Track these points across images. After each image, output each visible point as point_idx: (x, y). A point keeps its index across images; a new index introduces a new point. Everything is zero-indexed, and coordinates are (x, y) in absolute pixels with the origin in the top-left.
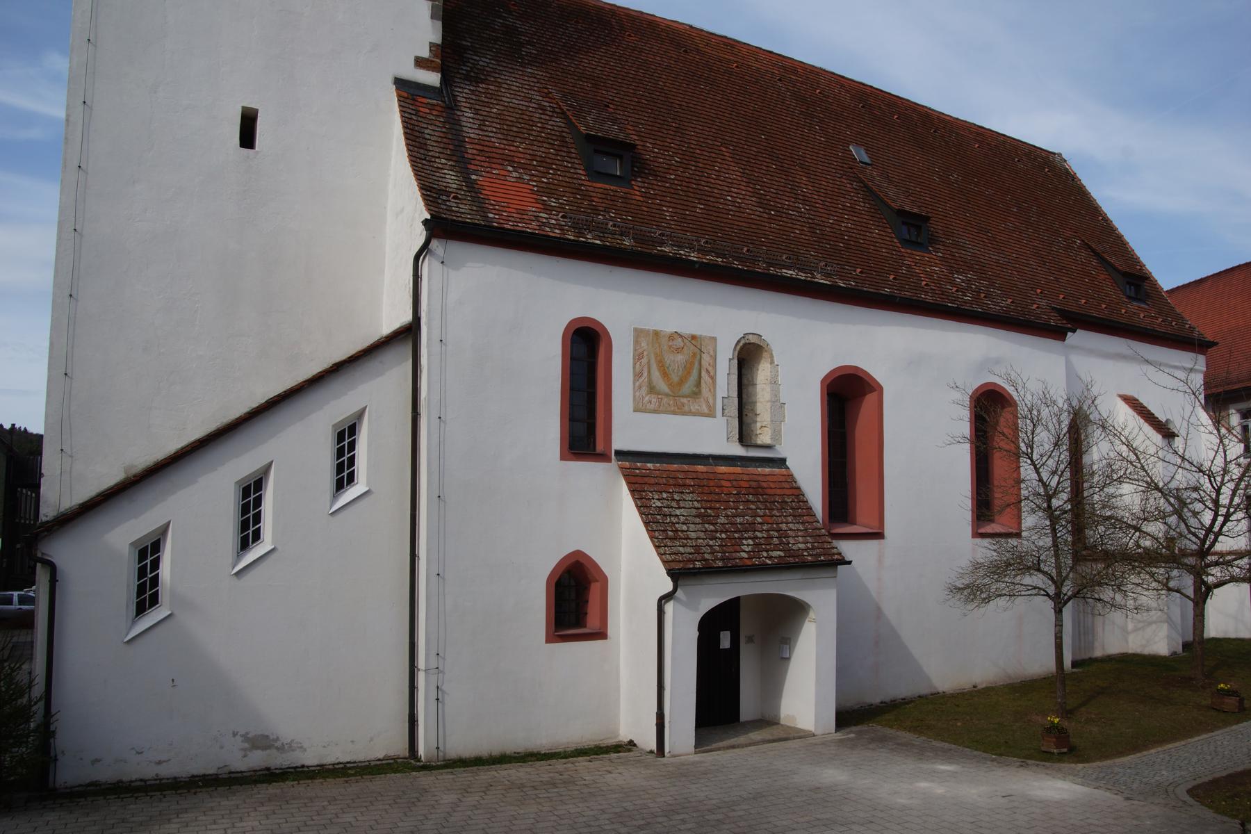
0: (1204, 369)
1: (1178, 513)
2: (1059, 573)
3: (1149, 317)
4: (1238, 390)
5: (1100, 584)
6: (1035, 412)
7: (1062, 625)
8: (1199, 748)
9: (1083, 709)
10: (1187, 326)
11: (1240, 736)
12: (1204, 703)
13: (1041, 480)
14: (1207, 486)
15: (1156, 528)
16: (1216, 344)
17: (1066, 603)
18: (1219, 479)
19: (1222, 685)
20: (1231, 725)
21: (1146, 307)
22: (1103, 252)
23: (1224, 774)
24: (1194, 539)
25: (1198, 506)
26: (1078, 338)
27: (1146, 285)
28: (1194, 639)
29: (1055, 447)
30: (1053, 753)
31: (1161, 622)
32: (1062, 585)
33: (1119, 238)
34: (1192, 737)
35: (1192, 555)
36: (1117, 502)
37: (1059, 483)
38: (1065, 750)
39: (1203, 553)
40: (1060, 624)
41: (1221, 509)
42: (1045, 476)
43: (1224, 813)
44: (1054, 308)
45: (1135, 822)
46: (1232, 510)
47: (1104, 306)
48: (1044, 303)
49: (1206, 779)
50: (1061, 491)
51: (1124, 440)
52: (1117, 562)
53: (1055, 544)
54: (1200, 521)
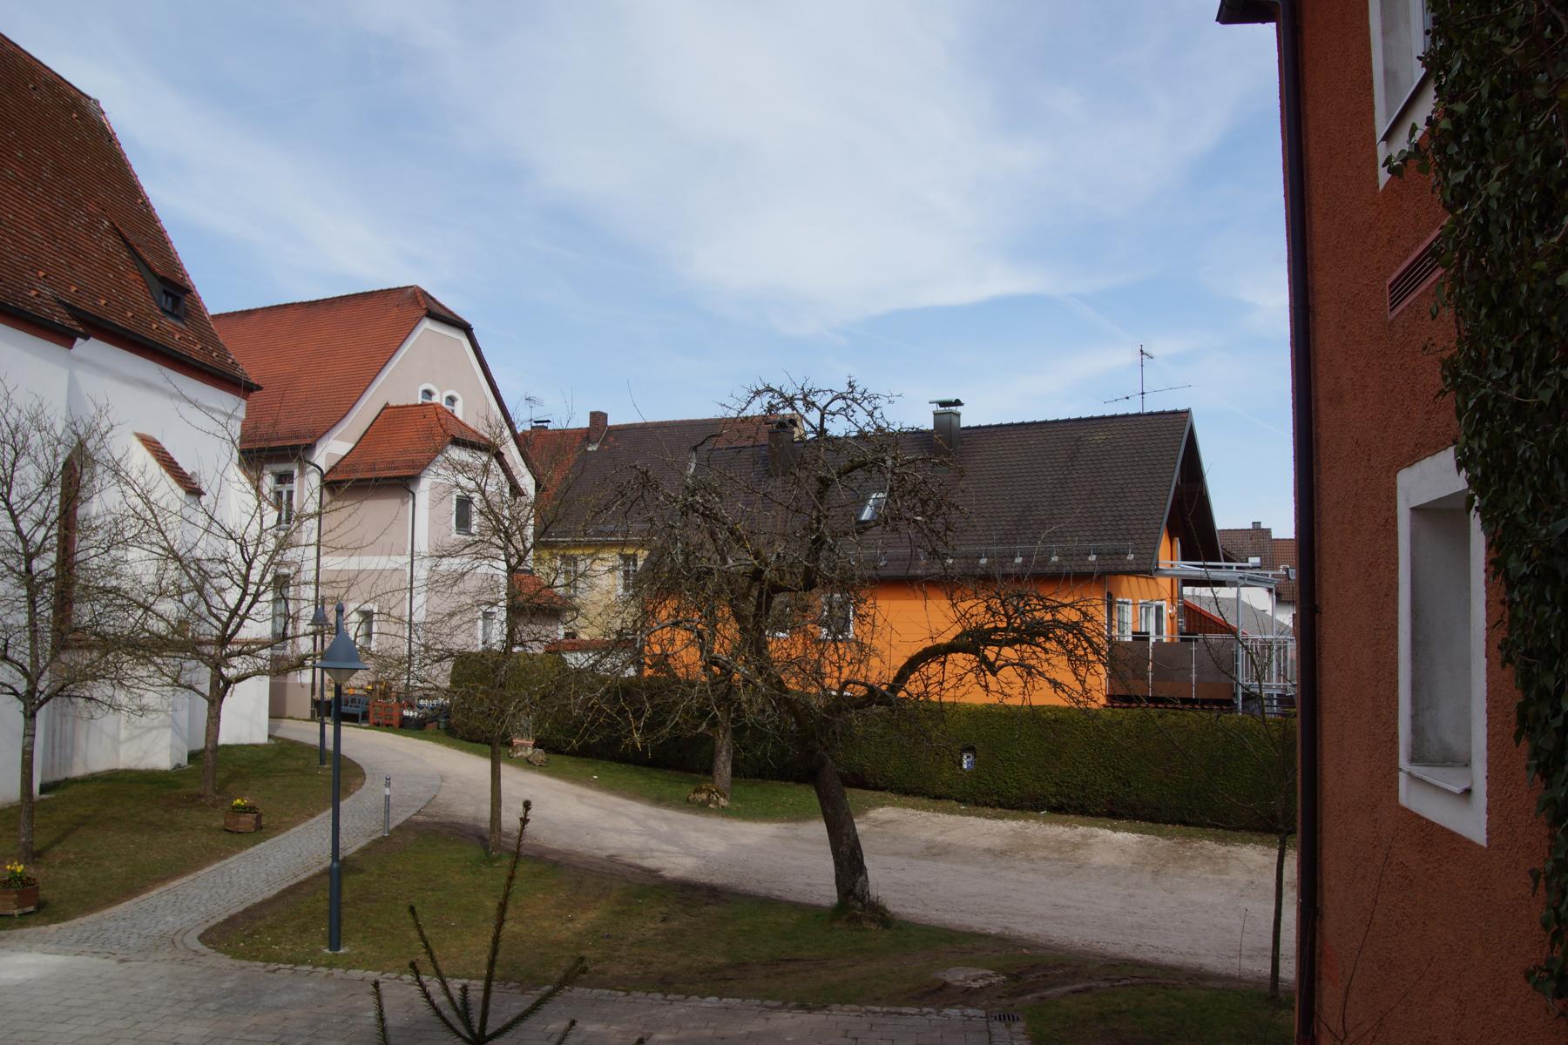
0: (244, 417)
1: (200, 590)
2: (35, 662)
3: (186, 340)
4: (284, 448)
5: (94, 678)
6: (19, 437)
7: (33, 736)
8: (212, 880)
9: (57, 848)
10: (230, 361)
11: (257, 860)
12: (215, 824)
13: (19, 532)
14: (237, 559)
15: (168, 607)
16: (261, 388)
17: (41, 704)
18: (251, 550)
19: (238, 801)
20: (247, 848)
21: (183, 326)
22: (138, 246)
23: (241, 908)
24: (216, 623)
25: (226, 582)
26: (90, 349)
27: (186, 300)
28: (206, 747)
29: (44, 488)
30: (13, 915)
31: (164, 727)
32: (38, 678)
33: (161, 233)
34: (202, 868)
35: (209, 643)
36: (127, 570)
37: (45, 539)
38: (31, 909)
39: (224, 640)
40: (32, 733)
41: (251, 586)
42: (26, 526)
43: (242, 957)
44: (60, 302)
45: (134, 991)
46: (262, 588)
47: (130, 314)
48: (47, 292)
49: (221, 919)
50: (49, 550)
51: (139, 491)
52: (119, 648)
53: (32, 623)
54: (224, 601)
